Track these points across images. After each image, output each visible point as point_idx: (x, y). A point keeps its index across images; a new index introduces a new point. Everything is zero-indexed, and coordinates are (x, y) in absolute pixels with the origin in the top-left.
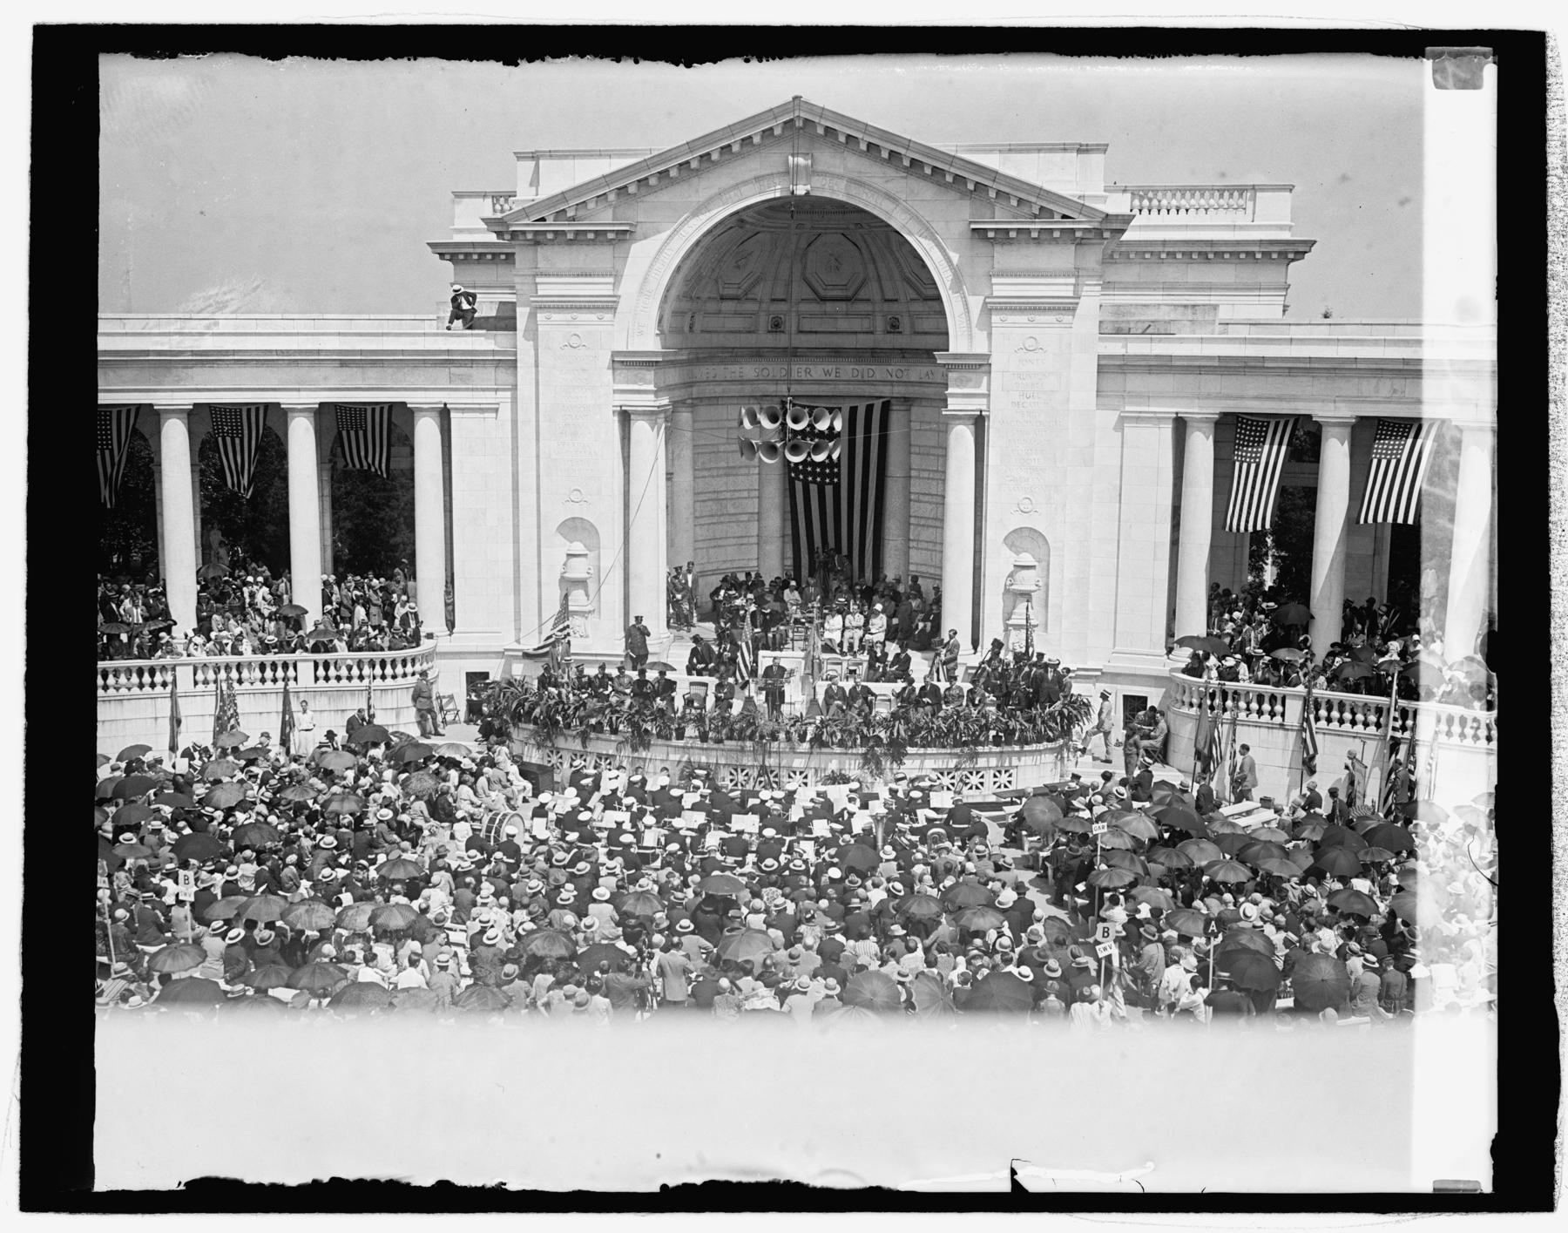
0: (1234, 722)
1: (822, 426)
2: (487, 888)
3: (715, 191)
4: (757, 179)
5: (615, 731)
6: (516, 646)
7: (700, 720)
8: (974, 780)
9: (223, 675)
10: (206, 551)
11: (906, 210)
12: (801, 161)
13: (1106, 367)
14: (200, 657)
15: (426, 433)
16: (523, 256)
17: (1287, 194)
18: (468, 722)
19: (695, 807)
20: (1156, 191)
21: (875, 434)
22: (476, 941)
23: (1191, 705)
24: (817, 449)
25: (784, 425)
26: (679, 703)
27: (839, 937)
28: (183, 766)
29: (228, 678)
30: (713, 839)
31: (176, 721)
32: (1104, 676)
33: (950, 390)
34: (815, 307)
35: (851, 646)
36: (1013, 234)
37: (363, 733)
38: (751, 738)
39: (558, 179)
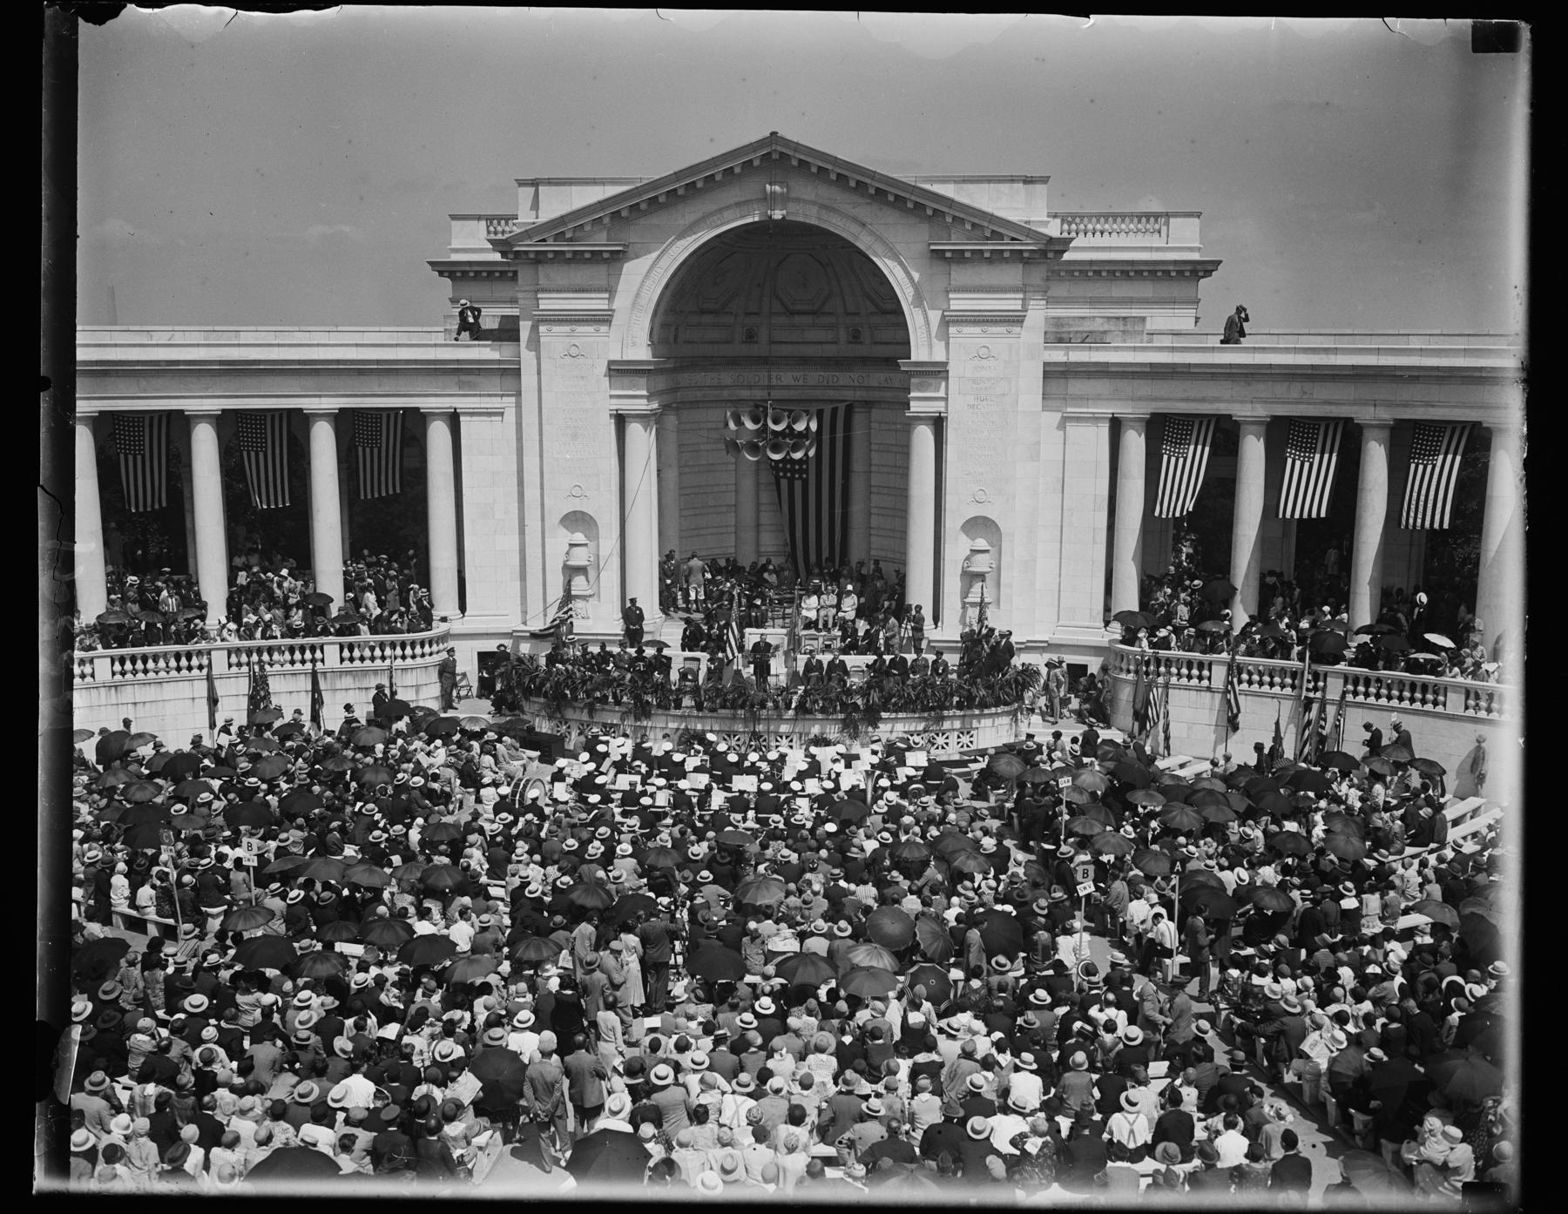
0: (1167, 686)
1: (800, 427)
2: (522, 847)
3: (699, 215)
4: (738, 204)
5: (618, 702)
6: (523, 628)
7: (695, 691)
8: (940, 740)
9: (255, 658)
10: (234, 547)
11: (872, 233)
12: (777, 188)
13: (1053, 373)
14: (234, 641)
15: (438, 435)
16: (525, 274)
18: (480, 696)
19: (697, 770)
20: (1082, 217)
21: (840, 435)
22: (517, 896)
23: (1129, 671)
24: (795, 448)
25: (765, 425)
26: (674, 676)
27: (842, 883)
28: (224, 740)
29: (260, 661)
30: (718, 799)
31: (213, 701)
32: (1049, 647)
33: (913, 394)
34: (782, 320)
35: (826, 624)
36: (967, 255)
37: (387, 708)
38: (742, 707)
39: (557, 204)
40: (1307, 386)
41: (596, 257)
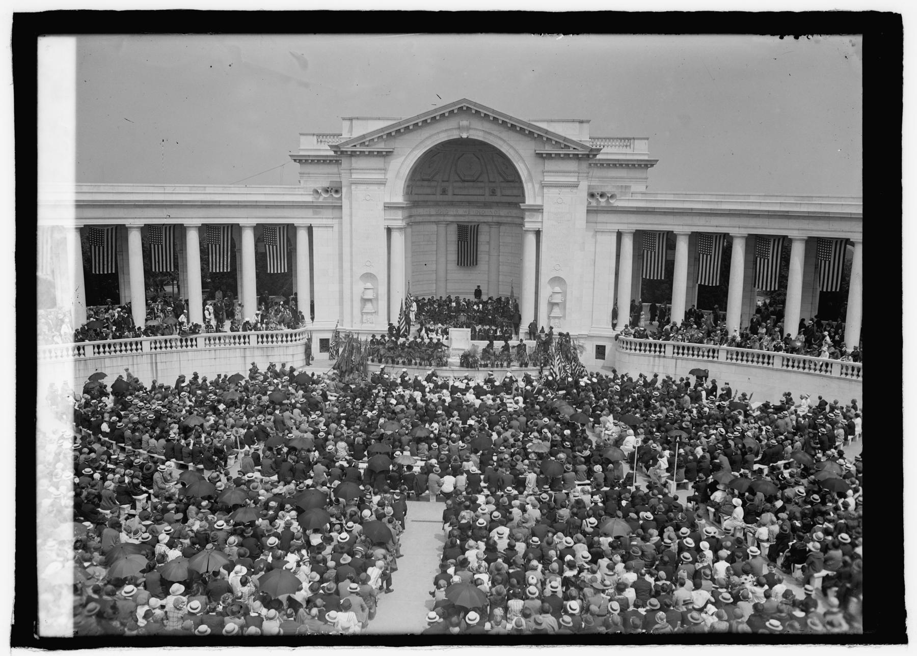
11: (508, 144)
15: (302, 238)
16: (345, 162)
17: (646, 141)
34: (460, 184)
39: (361, 129)
40: (708, 218)
41: (380, 154)
